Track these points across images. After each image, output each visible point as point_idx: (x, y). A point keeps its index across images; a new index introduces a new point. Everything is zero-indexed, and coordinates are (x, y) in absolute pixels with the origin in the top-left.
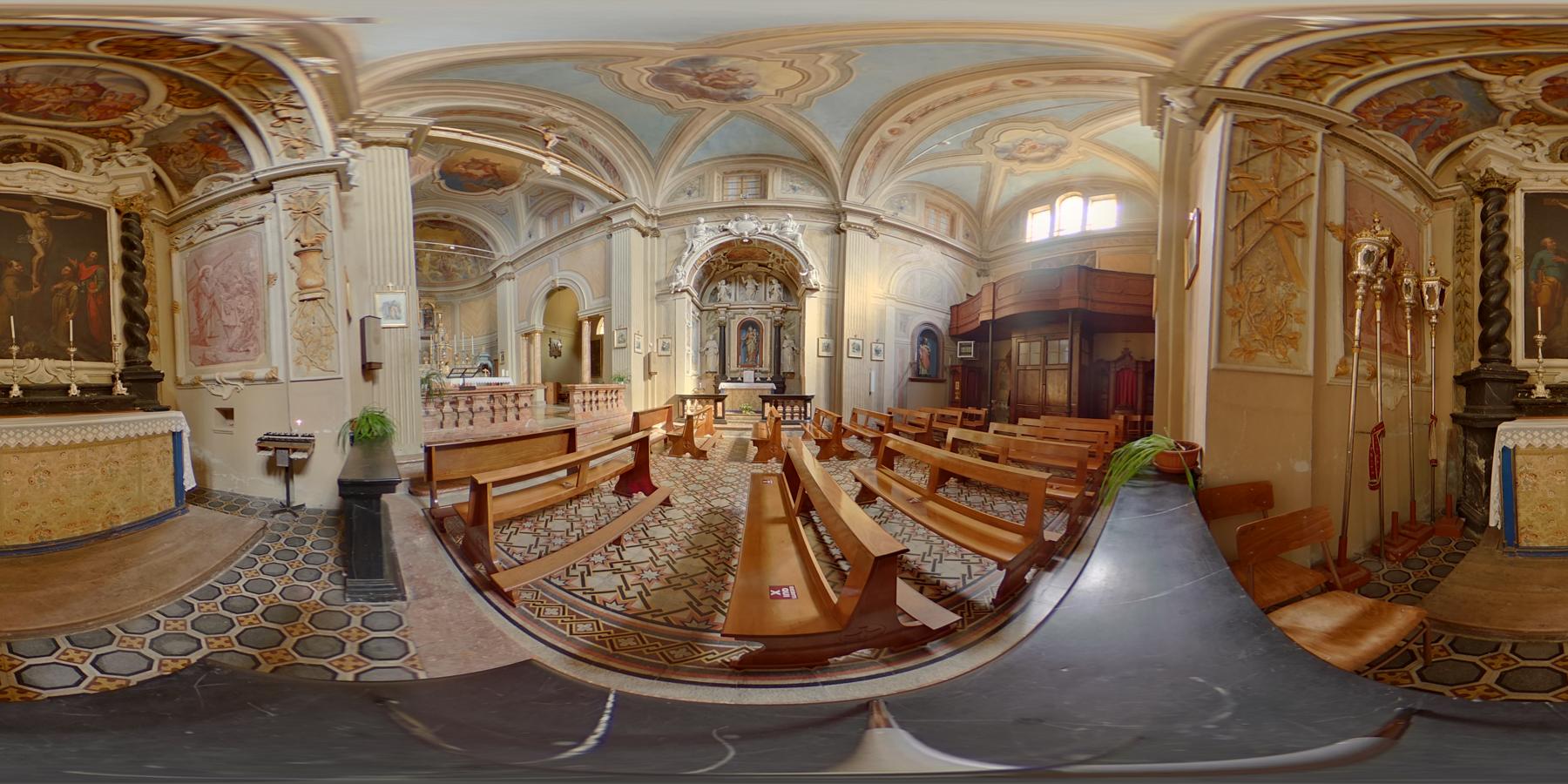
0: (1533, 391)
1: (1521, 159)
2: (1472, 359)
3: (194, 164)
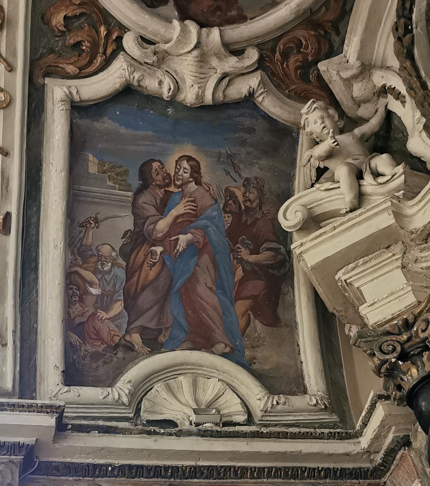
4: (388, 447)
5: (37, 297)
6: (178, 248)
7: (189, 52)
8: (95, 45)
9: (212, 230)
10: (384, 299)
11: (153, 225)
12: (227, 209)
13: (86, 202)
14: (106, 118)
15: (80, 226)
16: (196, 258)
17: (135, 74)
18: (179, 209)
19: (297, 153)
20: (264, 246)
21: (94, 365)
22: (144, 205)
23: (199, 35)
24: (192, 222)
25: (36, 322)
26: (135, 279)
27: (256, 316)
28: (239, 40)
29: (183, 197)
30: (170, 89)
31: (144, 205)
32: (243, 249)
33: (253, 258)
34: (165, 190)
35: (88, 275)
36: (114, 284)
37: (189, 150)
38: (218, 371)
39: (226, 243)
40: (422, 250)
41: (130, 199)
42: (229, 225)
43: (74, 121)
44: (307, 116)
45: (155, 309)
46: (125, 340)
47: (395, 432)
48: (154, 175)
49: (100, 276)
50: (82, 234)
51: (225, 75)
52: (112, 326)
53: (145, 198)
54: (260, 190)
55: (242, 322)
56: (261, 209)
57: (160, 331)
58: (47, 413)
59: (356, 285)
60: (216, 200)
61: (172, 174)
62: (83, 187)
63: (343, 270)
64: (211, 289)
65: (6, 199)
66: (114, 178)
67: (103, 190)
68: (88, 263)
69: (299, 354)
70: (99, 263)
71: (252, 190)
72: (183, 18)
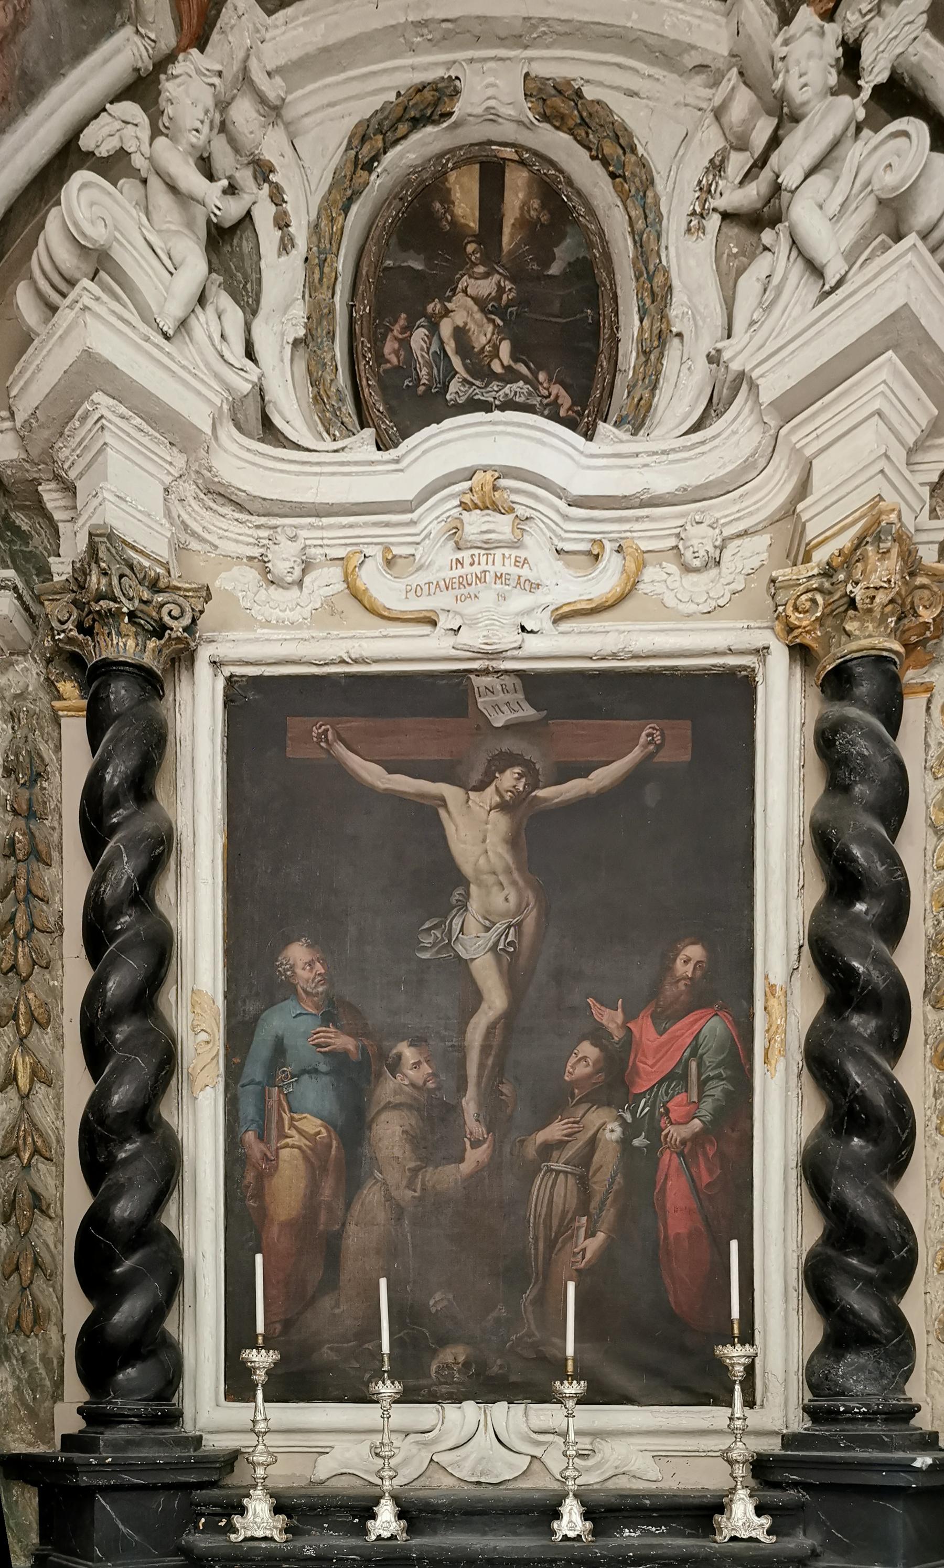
0: (237, 1520)
2: (57, 1395)
10: (136, 509)
59: (107, 437)
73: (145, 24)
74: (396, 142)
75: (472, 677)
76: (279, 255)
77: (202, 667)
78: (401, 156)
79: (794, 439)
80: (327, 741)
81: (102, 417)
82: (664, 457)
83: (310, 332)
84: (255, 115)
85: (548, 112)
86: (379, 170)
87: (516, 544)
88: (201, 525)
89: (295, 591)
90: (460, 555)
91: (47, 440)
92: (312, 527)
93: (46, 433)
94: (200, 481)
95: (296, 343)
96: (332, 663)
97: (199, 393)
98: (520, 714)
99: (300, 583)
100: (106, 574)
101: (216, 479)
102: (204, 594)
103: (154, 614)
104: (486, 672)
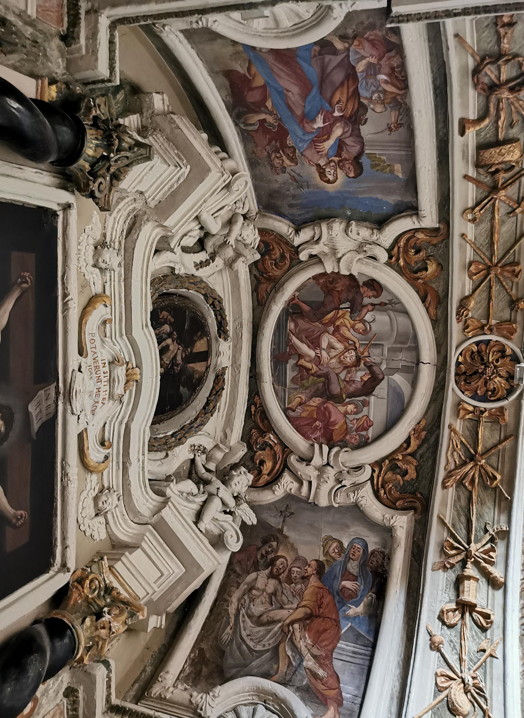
1: (169, 222)
3: (272, 622)
4: (80, 27)
5: (432, 68)
6: (322, 117)
7: (343, 255)
8: (406, 252)
9: (300, 133)
10: (145, 175)
11: (345, 130)
12: (292, 149)
13: (400, 142)
14: (393, 203)
15: (403, 124)
16: (306, 112)
17: (376, 238)
18: (328, 145)
19: (255, 195)
20: (257, 127)
21: (371, 20)
22: (355, 145)
23: (339, 267)
24: (316, 137)
25: (430, 47)
26: (351, 90)
27: (244, 76)
28: (313, 266)
29: (327, 154)
30: (351, 232)
31: (355, 145)
32: (272, 122)
33: (262, 116)
34: (341, 157)
35: (390, 88)
36: (367, 84)
37: (329, 187)
38: (260, 36)
39: (286, 125)
40: (134, 209)
41: (366, 148)
42: (288, 138)
43: (415, 200)
44: (255, 237)
45: (329, 69)
46: (349, 43)
47: (80, 49)
48: (351, 167)
49: (380, 89)
50: (400, 118)
51: (317, 242)
52: (362, 52)
53: (355, 150)
54: (273, 166)
55: (254, 70)
56: (268, 153)
57: (320, 53)
58: (401, 15)
59: (172, 168)
60: (302, 155)
61: (338, 170)
62: (404, 153)
63: (186, 175)
64: (288, 91)
65: (464, 145)
66: (381, 162)
67: (388, 152)
68: (391, 98)
69: (197, 54)
70: (382, 98)
71: (278, 165)
72: (351, 276)
73: (260, 218)
74: (216, 315)
75: (55, 384)
76: (194, 262)
77: (65, 197)
78: (211, 317)
79: (148, 534)
80: (22, 283)
81: (181, 168)
82: (141, 469)
83: (178, 276)
84: (229, 256)
85: (219, 377)
86: (210, 308)
87: (111, 396)
88: (122, 208)
89: (91, 262)
90: (107, 365)
91: (164, 130)
92: (120, 276)
93: (168, 131)
94: (141, 212)
95: (173, 269)
96: (64, 288)
97: (179, 222)
98: (35, 422)
99: (95, 266)
100: (130, 148)
101: (143, 222)
102: (106, 208)
103: (101, 172)
104: (57, 393)
